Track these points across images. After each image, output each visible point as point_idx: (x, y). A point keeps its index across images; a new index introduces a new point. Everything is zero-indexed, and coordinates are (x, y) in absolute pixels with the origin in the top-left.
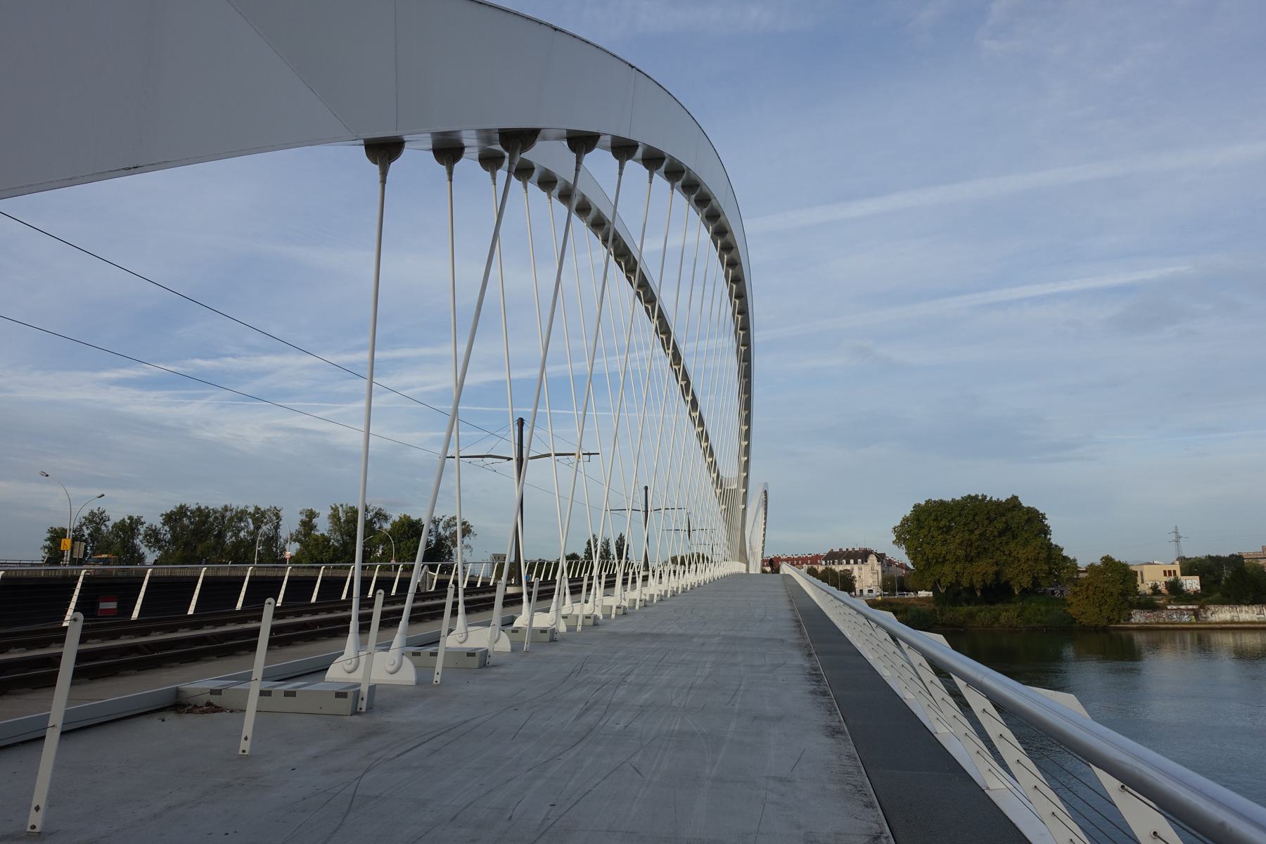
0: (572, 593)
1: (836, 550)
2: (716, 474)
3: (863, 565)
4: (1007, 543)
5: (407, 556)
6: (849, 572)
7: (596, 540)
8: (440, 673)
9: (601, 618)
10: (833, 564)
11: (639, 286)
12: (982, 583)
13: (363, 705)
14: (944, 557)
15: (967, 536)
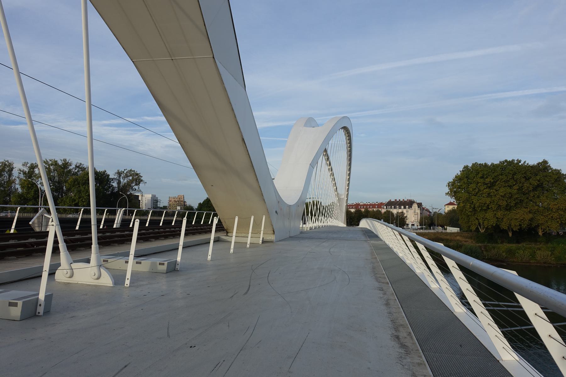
1: (393, 200)
3: (409, 210)
10: (391, 208)
12: (519, 227)
13: (41, 310)
14: (488, 206)
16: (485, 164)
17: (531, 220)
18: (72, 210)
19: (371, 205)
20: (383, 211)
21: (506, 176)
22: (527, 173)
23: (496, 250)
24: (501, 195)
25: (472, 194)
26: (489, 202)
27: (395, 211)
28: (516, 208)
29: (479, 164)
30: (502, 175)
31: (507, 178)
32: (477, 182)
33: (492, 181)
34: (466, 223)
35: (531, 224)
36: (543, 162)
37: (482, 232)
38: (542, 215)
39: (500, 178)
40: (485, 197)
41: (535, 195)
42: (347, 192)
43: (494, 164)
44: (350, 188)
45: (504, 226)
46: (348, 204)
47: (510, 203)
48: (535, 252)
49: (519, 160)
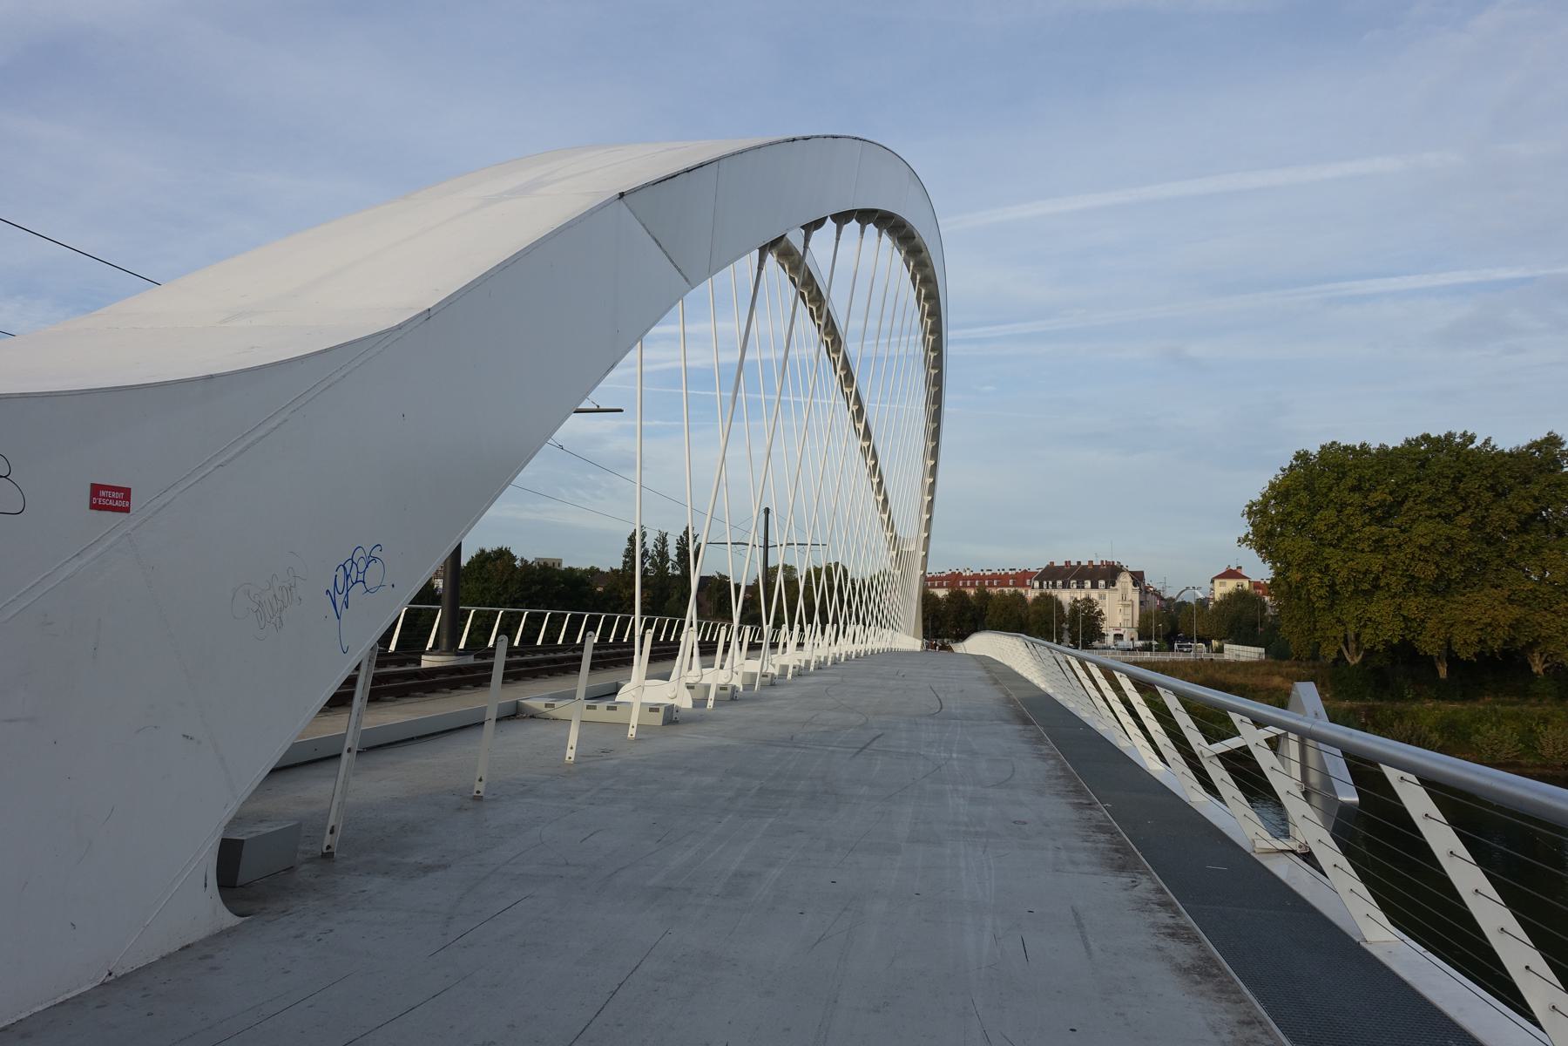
0: (702, 654)
1: (1059, 563)
2: (895, 552)
3: (1107, 591)
6: (1088, 599)
7: (644, 535)
8: (569, 748)
9: (741, 690)
10: (1054, 586)
11: (804, 285)
14: (1377, 578)
16: (1362, 446)
17: (1516, 625)
20: (1031, 594)
21: (1432, 483)
22: (1499, 474)
23: (1410, 724)
24: (1421, 544)
25: (1326, 542)
26: (1381, 569)
27: (1066, 596)
28: (1464, 588)
29: (1344, 447)
30: (1418, 480)
31: (1437, 490)
32: (1341, 505)
33: (1390, 498)
34: (1303, 633)
35: (1513, 639)
36: (1546, 439)
37: (1353, 663)
38: (1545, 609)
39: (1414, 490)
40: (1366, 550)
41: (1524, 544)
42: (921, 569)
44: (934, 519)
45: (1429, 645)
46: (928, 576)
47: (1447, 569)
48: (1531, 731)
49: (1469, 434)
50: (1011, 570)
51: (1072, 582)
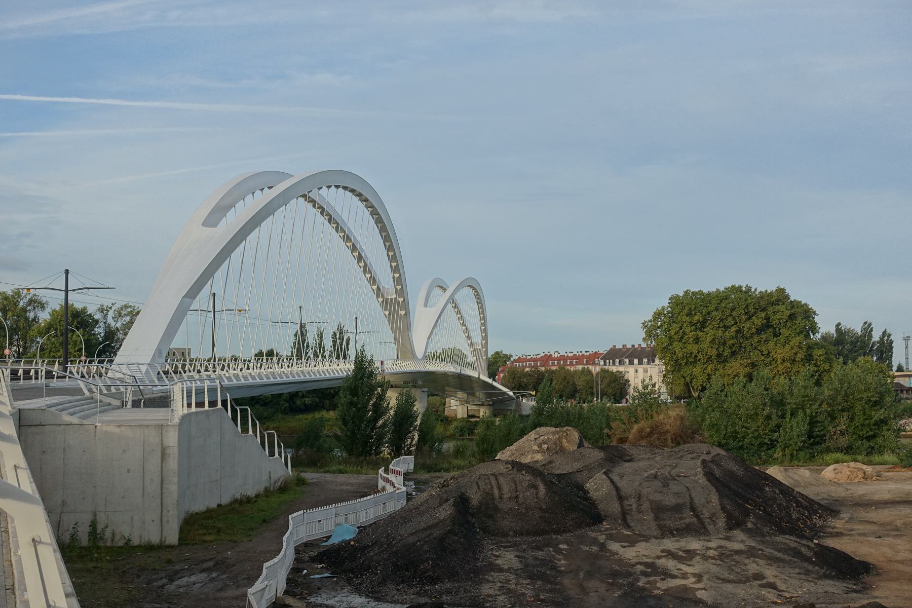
1: (619, 346)
3: (649, 366)
4: (767, 341)
5: (73, 352)
10: (614, 364)
14: (696, 356)
15: (720, 333)
18: (336, 573)
19: (575, 357)
26: (697, 352)
43: (678, 296)
50: (586, 352)
51: (625, 360)
